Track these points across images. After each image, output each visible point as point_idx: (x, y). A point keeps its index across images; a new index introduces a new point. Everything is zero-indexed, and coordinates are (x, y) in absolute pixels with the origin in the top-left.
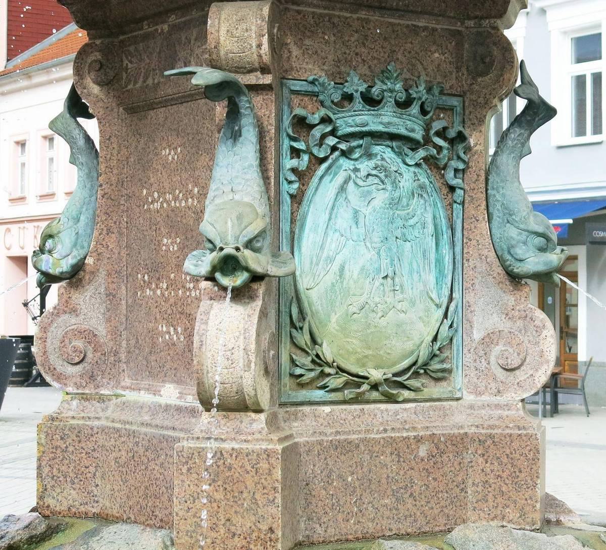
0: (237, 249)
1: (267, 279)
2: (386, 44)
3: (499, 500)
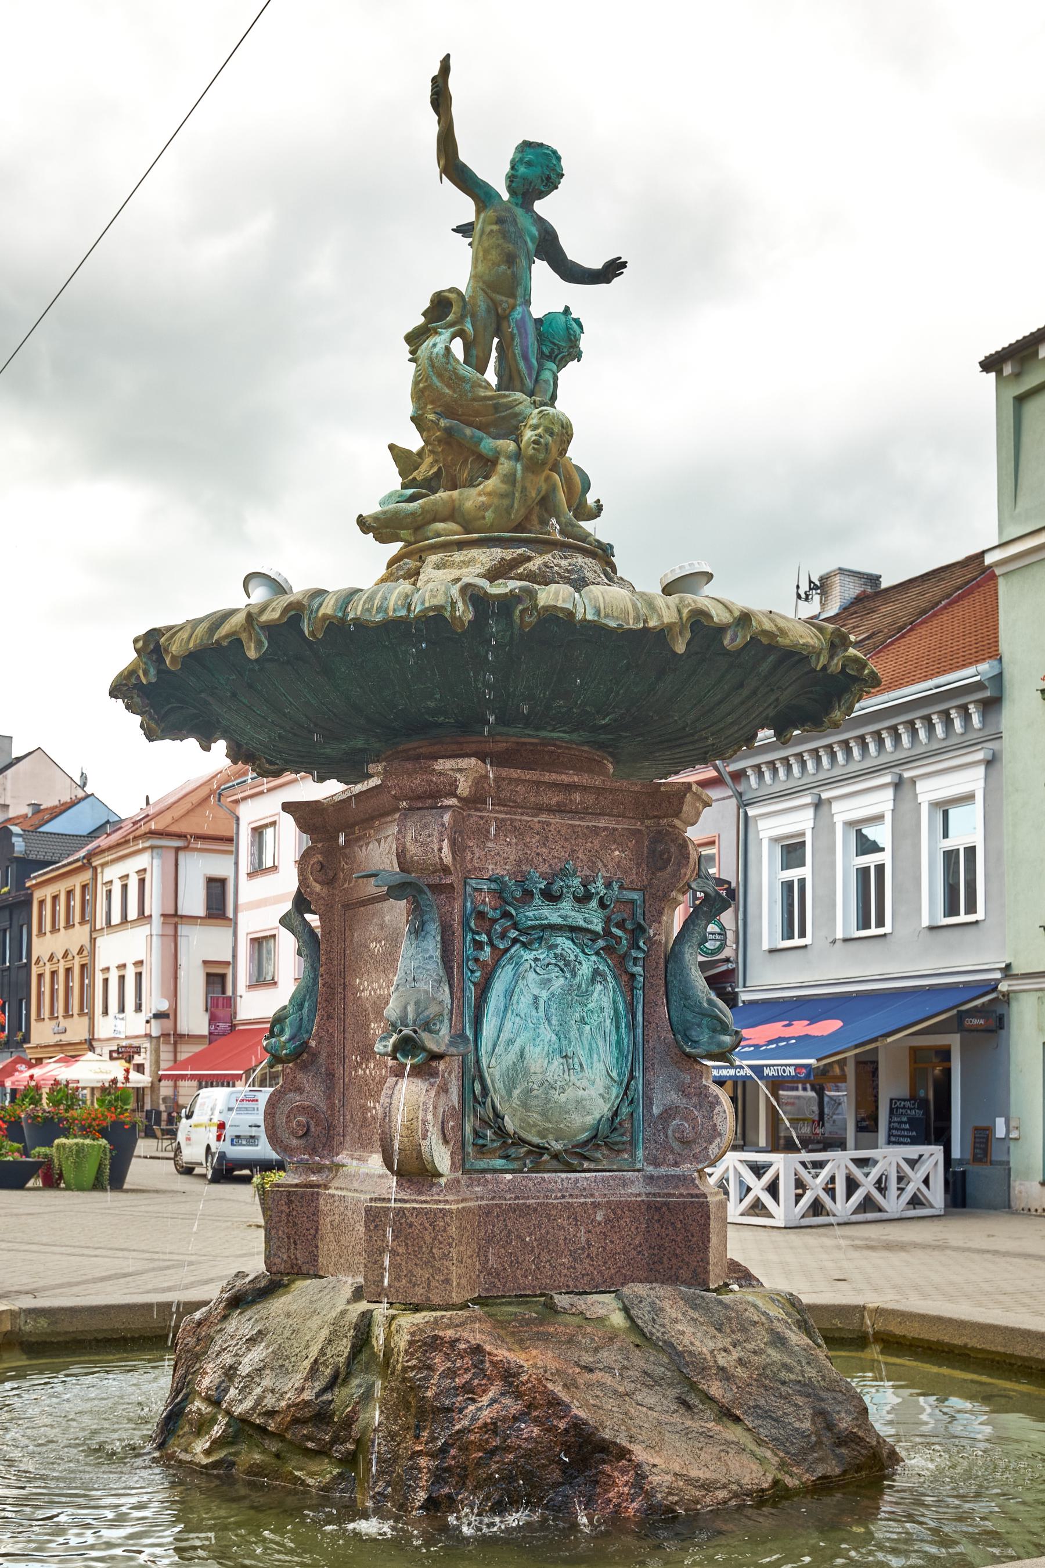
0: (415, 1032)
1: (447, 1058)
2: (566, 844)
3: (674, 1261)
